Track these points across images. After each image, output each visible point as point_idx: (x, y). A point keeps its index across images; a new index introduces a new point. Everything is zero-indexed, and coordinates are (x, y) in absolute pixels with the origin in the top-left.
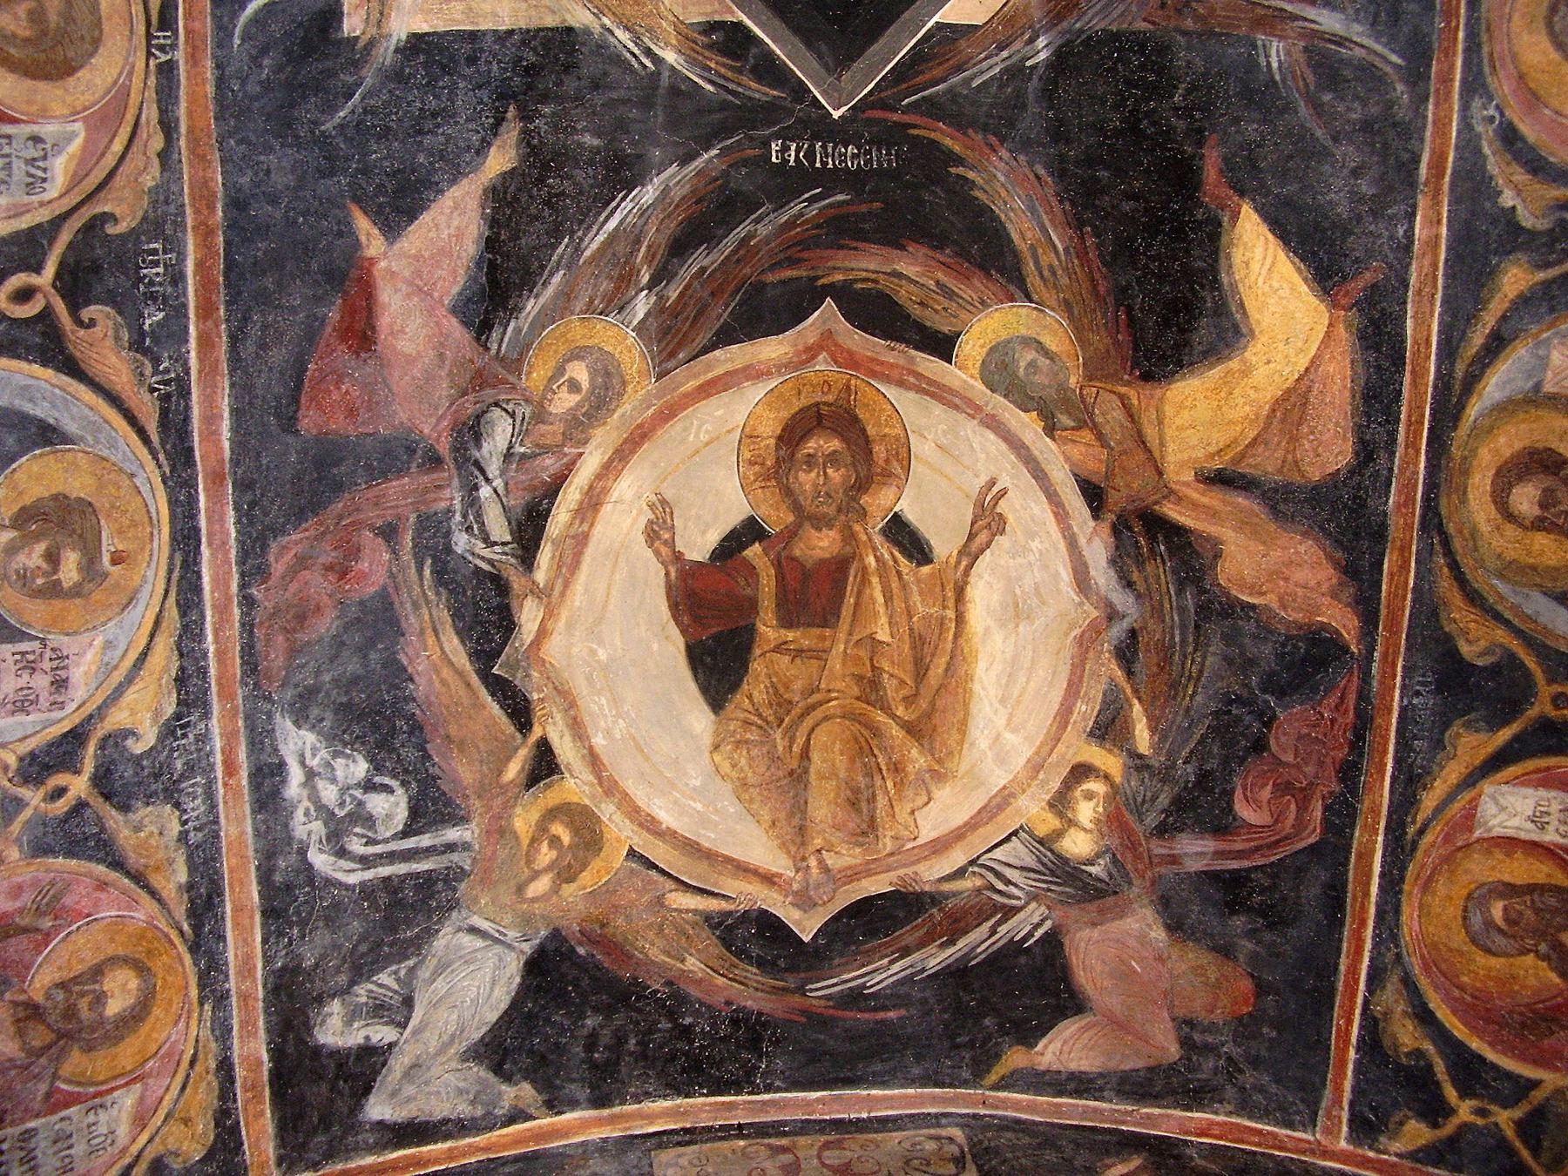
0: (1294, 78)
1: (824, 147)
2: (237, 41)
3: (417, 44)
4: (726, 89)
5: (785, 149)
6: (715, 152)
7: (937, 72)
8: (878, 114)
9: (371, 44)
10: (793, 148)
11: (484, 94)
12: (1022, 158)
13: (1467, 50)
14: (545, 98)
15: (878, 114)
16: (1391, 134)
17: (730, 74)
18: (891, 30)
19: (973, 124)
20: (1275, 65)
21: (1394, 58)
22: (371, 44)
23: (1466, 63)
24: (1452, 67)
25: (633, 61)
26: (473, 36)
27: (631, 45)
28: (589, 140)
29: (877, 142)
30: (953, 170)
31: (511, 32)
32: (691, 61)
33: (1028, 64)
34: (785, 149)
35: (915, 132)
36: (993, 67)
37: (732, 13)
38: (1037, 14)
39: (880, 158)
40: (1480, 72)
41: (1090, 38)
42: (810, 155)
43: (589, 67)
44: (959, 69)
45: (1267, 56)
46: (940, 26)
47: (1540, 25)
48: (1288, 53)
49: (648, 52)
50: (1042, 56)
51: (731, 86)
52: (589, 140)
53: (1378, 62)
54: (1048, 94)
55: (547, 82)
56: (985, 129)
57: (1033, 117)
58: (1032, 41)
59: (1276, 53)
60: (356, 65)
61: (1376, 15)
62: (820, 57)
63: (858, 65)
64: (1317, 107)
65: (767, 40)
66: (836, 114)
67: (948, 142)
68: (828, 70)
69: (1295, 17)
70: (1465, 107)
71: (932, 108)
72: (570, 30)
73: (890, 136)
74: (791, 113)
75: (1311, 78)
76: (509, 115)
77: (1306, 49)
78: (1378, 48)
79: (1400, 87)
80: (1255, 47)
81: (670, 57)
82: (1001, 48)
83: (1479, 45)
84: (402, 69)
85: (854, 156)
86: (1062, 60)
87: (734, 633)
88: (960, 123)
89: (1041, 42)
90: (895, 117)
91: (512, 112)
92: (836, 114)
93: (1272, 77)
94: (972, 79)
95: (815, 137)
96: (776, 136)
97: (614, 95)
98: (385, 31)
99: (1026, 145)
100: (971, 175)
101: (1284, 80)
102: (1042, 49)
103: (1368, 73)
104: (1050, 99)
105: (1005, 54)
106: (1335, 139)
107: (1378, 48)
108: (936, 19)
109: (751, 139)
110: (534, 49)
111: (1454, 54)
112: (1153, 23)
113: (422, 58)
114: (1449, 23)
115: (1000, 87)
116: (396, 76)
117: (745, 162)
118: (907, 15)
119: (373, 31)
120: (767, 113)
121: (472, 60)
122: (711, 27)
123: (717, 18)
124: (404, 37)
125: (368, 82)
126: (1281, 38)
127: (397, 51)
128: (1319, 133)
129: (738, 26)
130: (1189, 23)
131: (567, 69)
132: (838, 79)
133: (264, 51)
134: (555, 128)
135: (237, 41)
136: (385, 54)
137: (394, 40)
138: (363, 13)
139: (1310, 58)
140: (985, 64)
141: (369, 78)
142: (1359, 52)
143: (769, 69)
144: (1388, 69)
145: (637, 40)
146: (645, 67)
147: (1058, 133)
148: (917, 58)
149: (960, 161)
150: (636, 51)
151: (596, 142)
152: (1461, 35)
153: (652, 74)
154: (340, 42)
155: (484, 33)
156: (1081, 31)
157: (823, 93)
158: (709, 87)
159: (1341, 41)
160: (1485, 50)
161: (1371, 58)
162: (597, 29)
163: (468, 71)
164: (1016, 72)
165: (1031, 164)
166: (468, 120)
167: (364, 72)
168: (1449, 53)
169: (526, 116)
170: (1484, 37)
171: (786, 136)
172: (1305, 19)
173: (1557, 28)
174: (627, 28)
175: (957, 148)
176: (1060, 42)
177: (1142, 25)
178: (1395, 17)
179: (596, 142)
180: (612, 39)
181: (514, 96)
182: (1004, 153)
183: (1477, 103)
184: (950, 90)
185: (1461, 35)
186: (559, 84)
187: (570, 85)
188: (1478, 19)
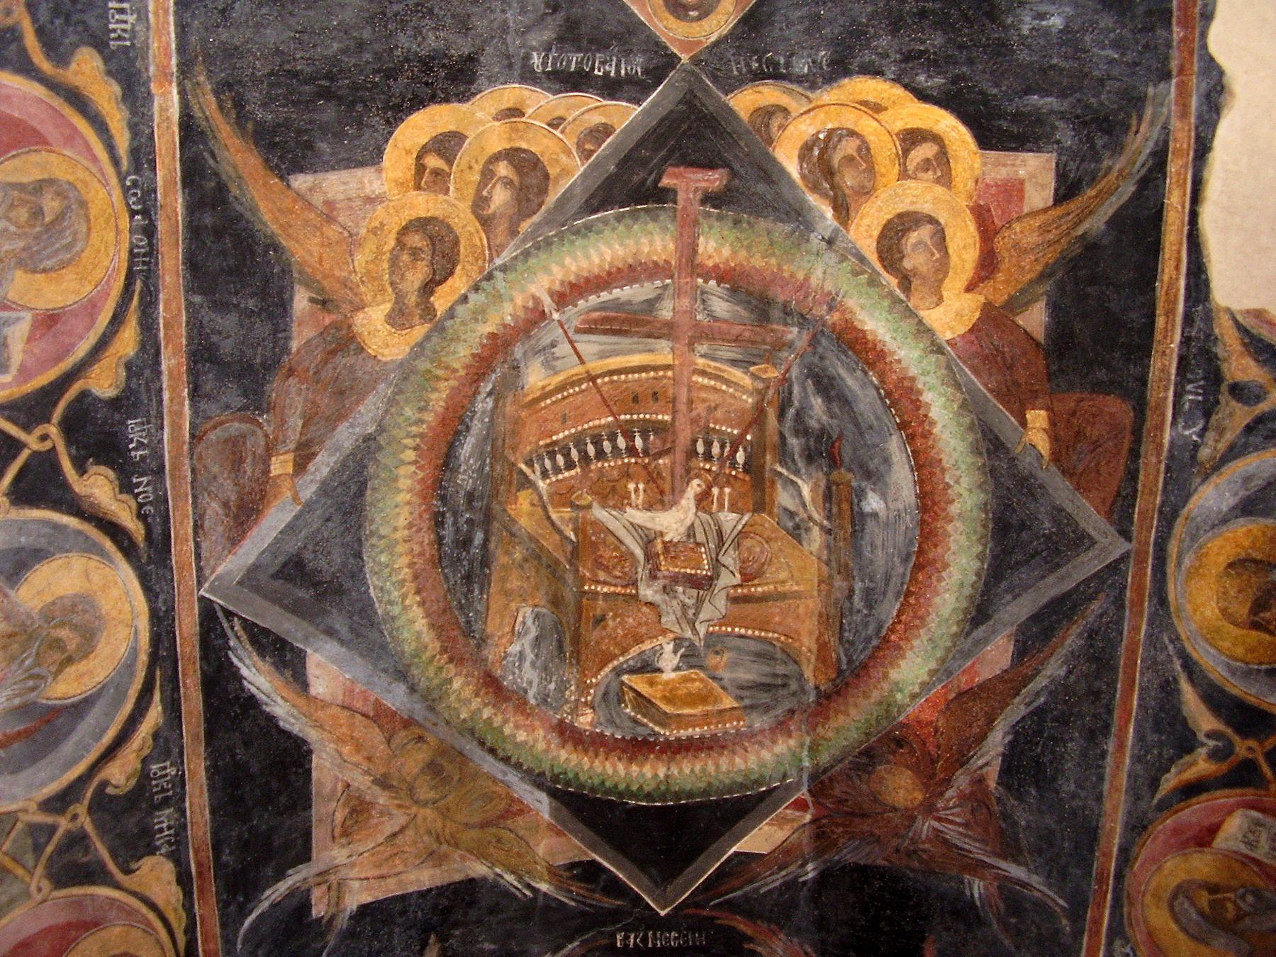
0: (991, 906)
1: (654, 934)
2: (239, 946)
3: (364, 911)
4: (584, 903)
5: (626, 938)
6: (576, 943)
7: (736, 883)
8: (691, 911)
9: (332, 918)
10: (632, 936)
11: (413, 932)
12: (795, 940)
13: (1113, 907)
14: (456, 925)
15: (691, 911)
16: (1057, 950)
17: (586, 894)
18: (700, 859)
19: (760, 917)
20: (976, 895)
21: (1061, 902)
22: (332, 918)
23: (1112, 915)
24: (1102, 916)
25: (518, 893)
26: (403, 898)
27: (516, 883)
28: (488, 946)
29: (692, 929)
30: (746, 946)
31: (430, 890)
32: (558, 888)
33: (801, 880)
34: (626, 938)
35: (719, 922)
36: (777, 880)
37: (586, 854)
38: (806, 850)
39: (698, 939)
40: (1121, 923)
41: (845, 867)
42: (645, 940)
43: (486, 900)
44: (751, 881)
45: (971, 889)
46: (736, 854)
47: (1165, 906)
48: (986, 888)
49: (529, 886)
50: (810, 875)
51: (589, 901)
52: (488, 946)
53: (1049, 902)
54: (815, 899)
55: (458, 915)
56: (769, 920)
57: (804, 910)
58: (803, 865)
59: (977, 888)
60: (322, 935)
61: (1050, 871)
62: (651, 877)
63: (680, 880)
64: (1006, 926)
65: (612, 869)
66: (663, 913)
67: (742, 927)
68: (655, 882)
69: (994, 867)
70: (1110, 943)
71: (731, 906)
72: (472, 880)
73: (699, 925)
74: (631, 914)
75: (1002, 906)
76: (431, 941)
77: (999, 887)
78: (1051, 893)
79: (1064, 922)
80: (962, 882)
81: (544, 887)
82: (780, 869)
83: (1122, 906)
84: (355, 929)
85: (675, 938)
86: (824, 878)
87: (1020, 851)
88: (751, 915)
89: (810, 867)
90: (705, 913)
91: (433, 938)
92: (663, 913)
93: (974, 903)
94: (760, 888)
95: (648, 928)
96: (620, 930)
97: (504, 916)
98: (342, 907)
99: (798, 931)
100: (759, 949)
101: (983, 906)
102: (811, 872)
103: (1042, 907)
104: (816, 903)
105: (783, 873)
106: (1017, 947)
107: (1051, 893)
108: (734, 849)
109: (602, 933)
110: (447, 898)
111: (1104, 907)
112: (890, 861)
113: (368, 919)
114: (1100, 887)
115: (781, 895)
116: (350, 934)
117: (597, 948)
118: (715, 846)
119: (332, 910)
120: (614, 916)
121: (403, 913)
122: (572, 866)
123: (577, 859)
124: (355, 908)
125: (332, 943)
126: (982, 879)
127: (351, 918)
128: (1007, 942)
129: (593, 862)
130: (916, 864)
131: (471, 904)
132: (664, 890)
133: (258, 946)
134: (464, 943)
135: (239, 946)
136: (342, 922)
137: (348, 913)
138: (326, 901)
139: (1001, 893)
140: (769, 879)
141: (332, 939)
142: (1036, 894)
143: (613, 887)
144: (1056, 908)
145: (520, 879)
146: (525, 895)
147: (821, 924)
148: (720, 874)
149: (750, 940)
150: (520, 886)
151: (492, 947)
152: (1109, 896)
153: (531, 899)
154: (309, 925)
155: (411, 894)
156: (839, 862)
157: (654, 900)
158: (573, 904)
159: (1024, 885)
160: (1125, 909)
161: (1045, 899)
162: (491, 876)
163: (401, 920)
164: (791, 885)
165: (801, 945)
166: (403, 950)
167: (329, 937)
168: (1100, 906)
169: (442, 939)
170: (1126, 902)
171: (627, 929)
172: (999, 868)
173: (1177, 909)
174: (513, 872)
175: (749, 933)
176: (821, 868)
177: (881, 862)
178: (1063, 875)
179: (492, 947)
180: (502, 881)
181: (434, 928)
182: (782, 936)
183: (1118, 943)
184: (745, 895)
185: (1109, 896)
186: (465, 914)
187: (473, 914)
188: (1122, 890)
